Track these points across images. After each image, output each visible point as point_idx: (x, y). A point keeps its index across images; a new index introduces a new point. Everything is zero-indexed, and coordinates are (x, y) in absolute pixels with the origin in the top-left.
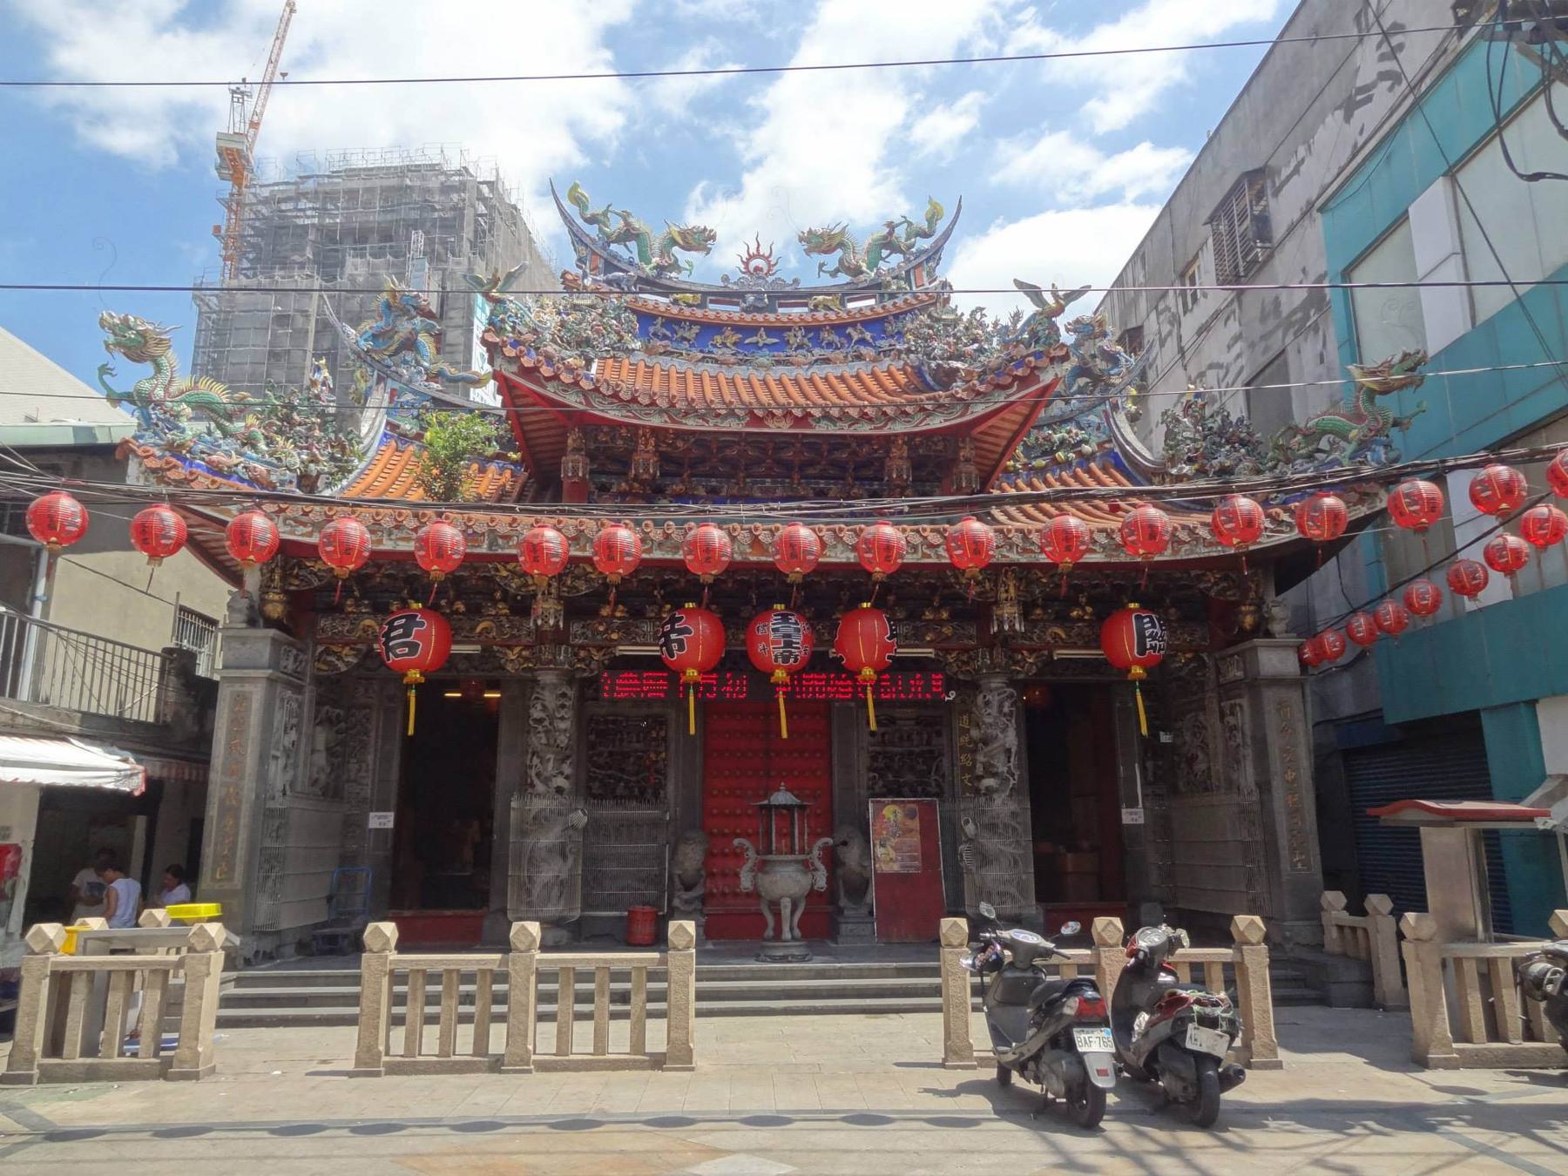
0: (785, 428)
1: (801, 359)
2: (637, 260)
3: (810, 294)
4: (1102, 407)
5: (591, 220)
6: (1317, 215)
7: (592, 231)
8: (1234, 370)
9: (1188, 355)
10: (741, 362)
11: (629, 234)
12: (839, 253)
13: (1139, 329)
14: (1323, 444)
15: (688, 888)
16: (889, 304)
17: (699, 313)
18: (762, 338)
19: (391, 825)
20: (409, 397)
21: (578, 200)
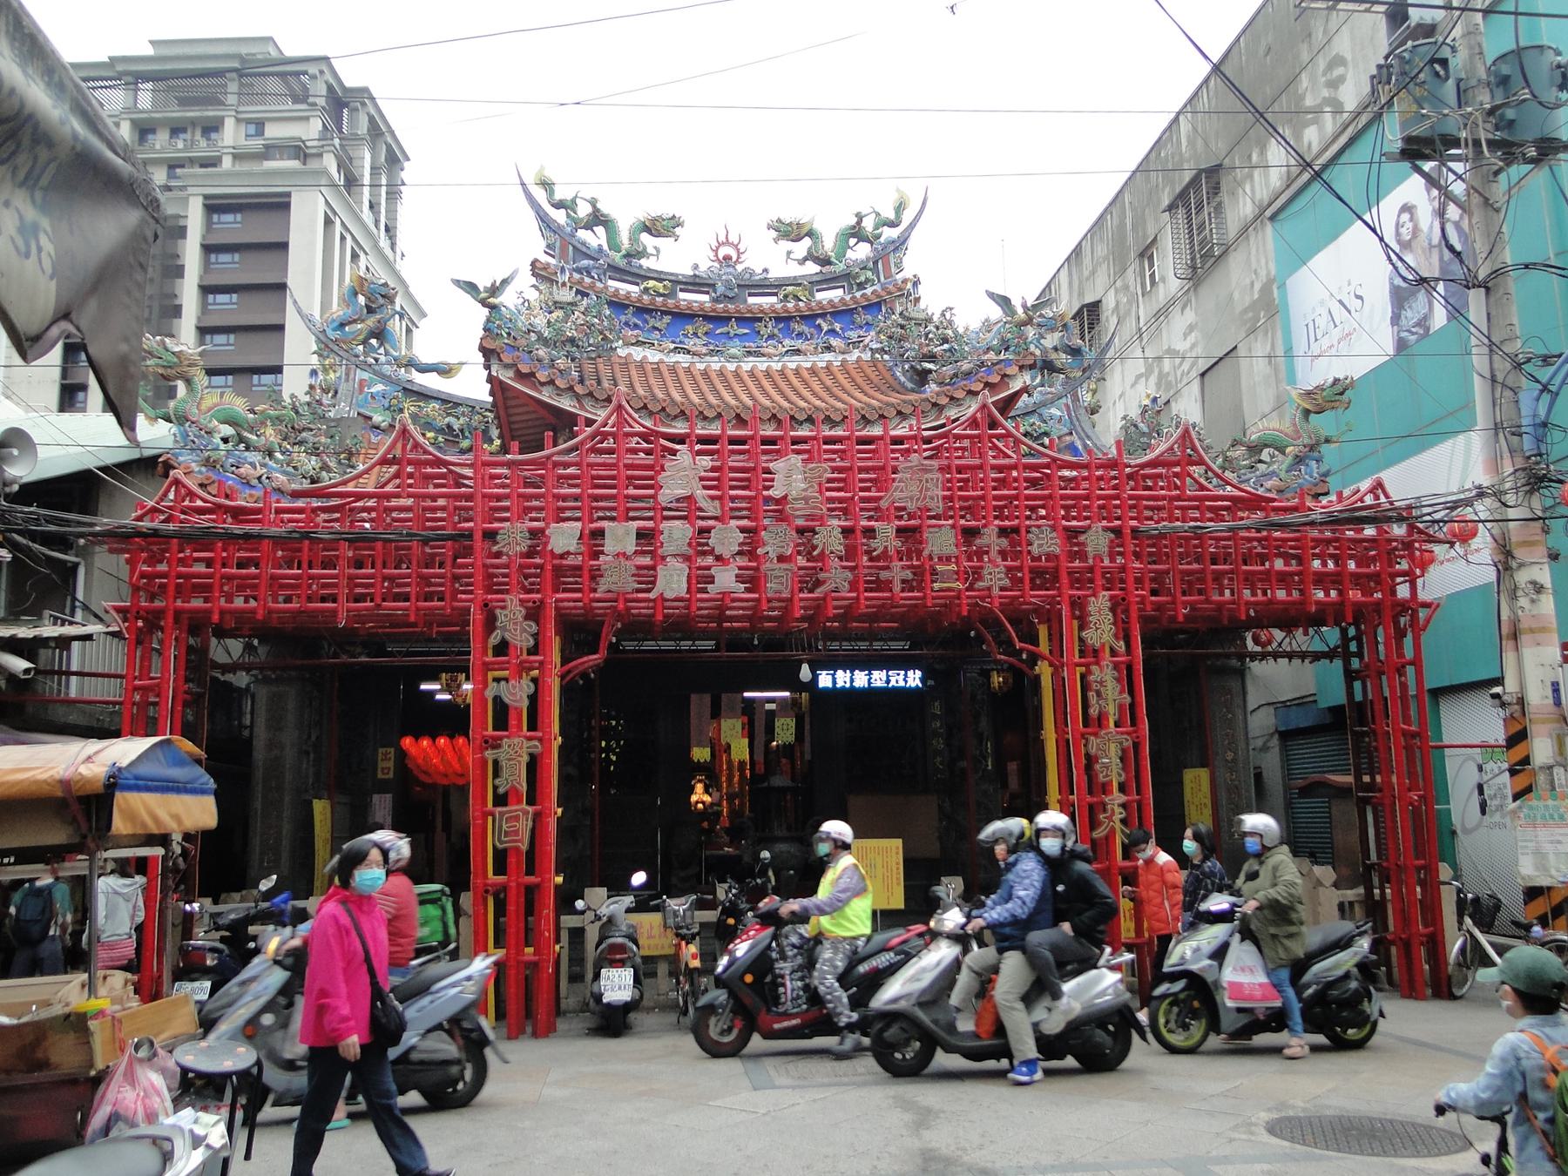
1: (771, 350)
2: (605, 247)
3: (779, 286)
4: (1064, 400)
5: (558, 205)
6: (1269, 227)
7: (560, 216)
10: (711, 353)
11: (598, 219)
12: (807, 242)
14: (1265, 456)
16: (858, 295)
20: (379, 388)
21: (547, 185)
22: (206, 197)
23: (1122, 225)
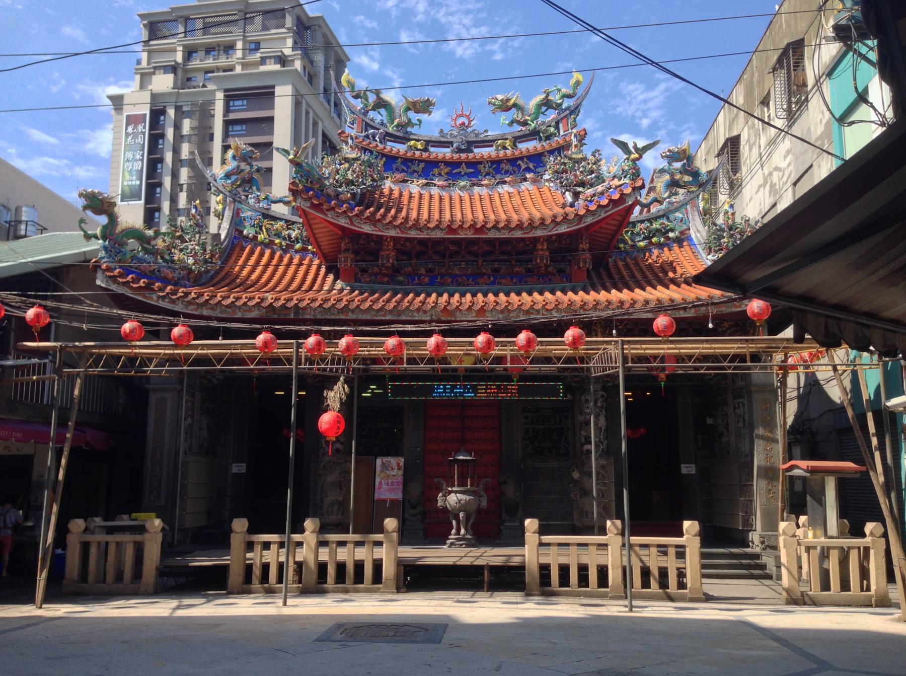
0: (470, 235)
3: (494, 141)
8: (787, 173)
9: (764, 159)
13: (738, 137)
15: (414, 507)
17: (425, 155)
18: (464, 169)
19: (244, 471)
22: (226, 91)
23: (752, 82)
